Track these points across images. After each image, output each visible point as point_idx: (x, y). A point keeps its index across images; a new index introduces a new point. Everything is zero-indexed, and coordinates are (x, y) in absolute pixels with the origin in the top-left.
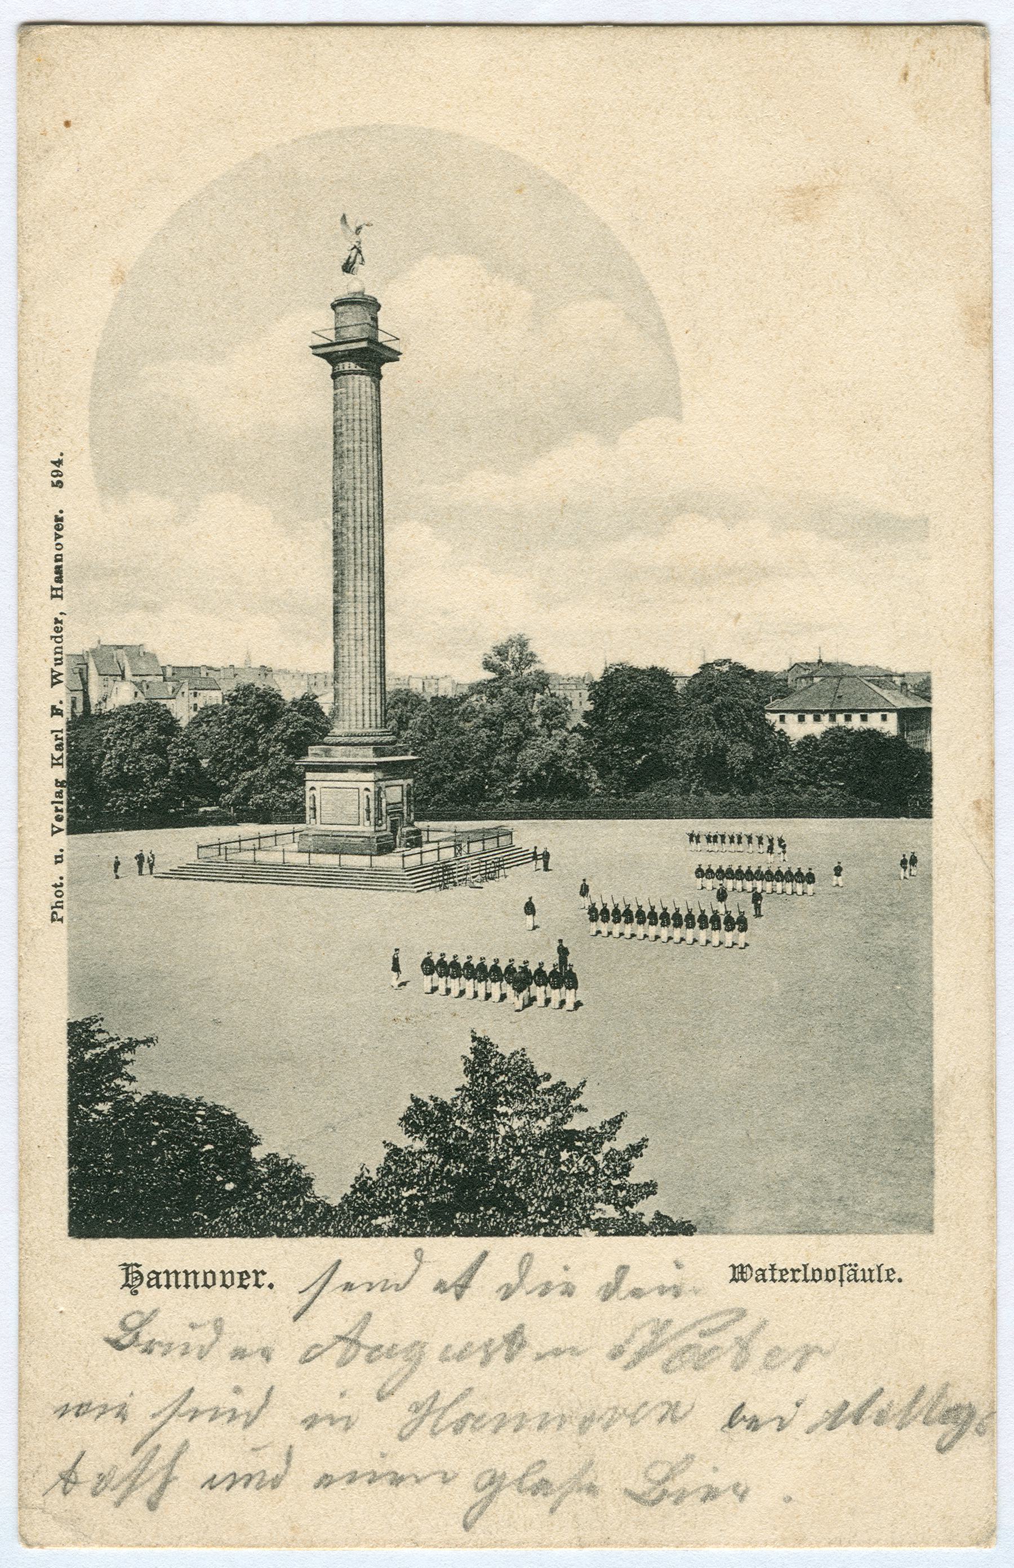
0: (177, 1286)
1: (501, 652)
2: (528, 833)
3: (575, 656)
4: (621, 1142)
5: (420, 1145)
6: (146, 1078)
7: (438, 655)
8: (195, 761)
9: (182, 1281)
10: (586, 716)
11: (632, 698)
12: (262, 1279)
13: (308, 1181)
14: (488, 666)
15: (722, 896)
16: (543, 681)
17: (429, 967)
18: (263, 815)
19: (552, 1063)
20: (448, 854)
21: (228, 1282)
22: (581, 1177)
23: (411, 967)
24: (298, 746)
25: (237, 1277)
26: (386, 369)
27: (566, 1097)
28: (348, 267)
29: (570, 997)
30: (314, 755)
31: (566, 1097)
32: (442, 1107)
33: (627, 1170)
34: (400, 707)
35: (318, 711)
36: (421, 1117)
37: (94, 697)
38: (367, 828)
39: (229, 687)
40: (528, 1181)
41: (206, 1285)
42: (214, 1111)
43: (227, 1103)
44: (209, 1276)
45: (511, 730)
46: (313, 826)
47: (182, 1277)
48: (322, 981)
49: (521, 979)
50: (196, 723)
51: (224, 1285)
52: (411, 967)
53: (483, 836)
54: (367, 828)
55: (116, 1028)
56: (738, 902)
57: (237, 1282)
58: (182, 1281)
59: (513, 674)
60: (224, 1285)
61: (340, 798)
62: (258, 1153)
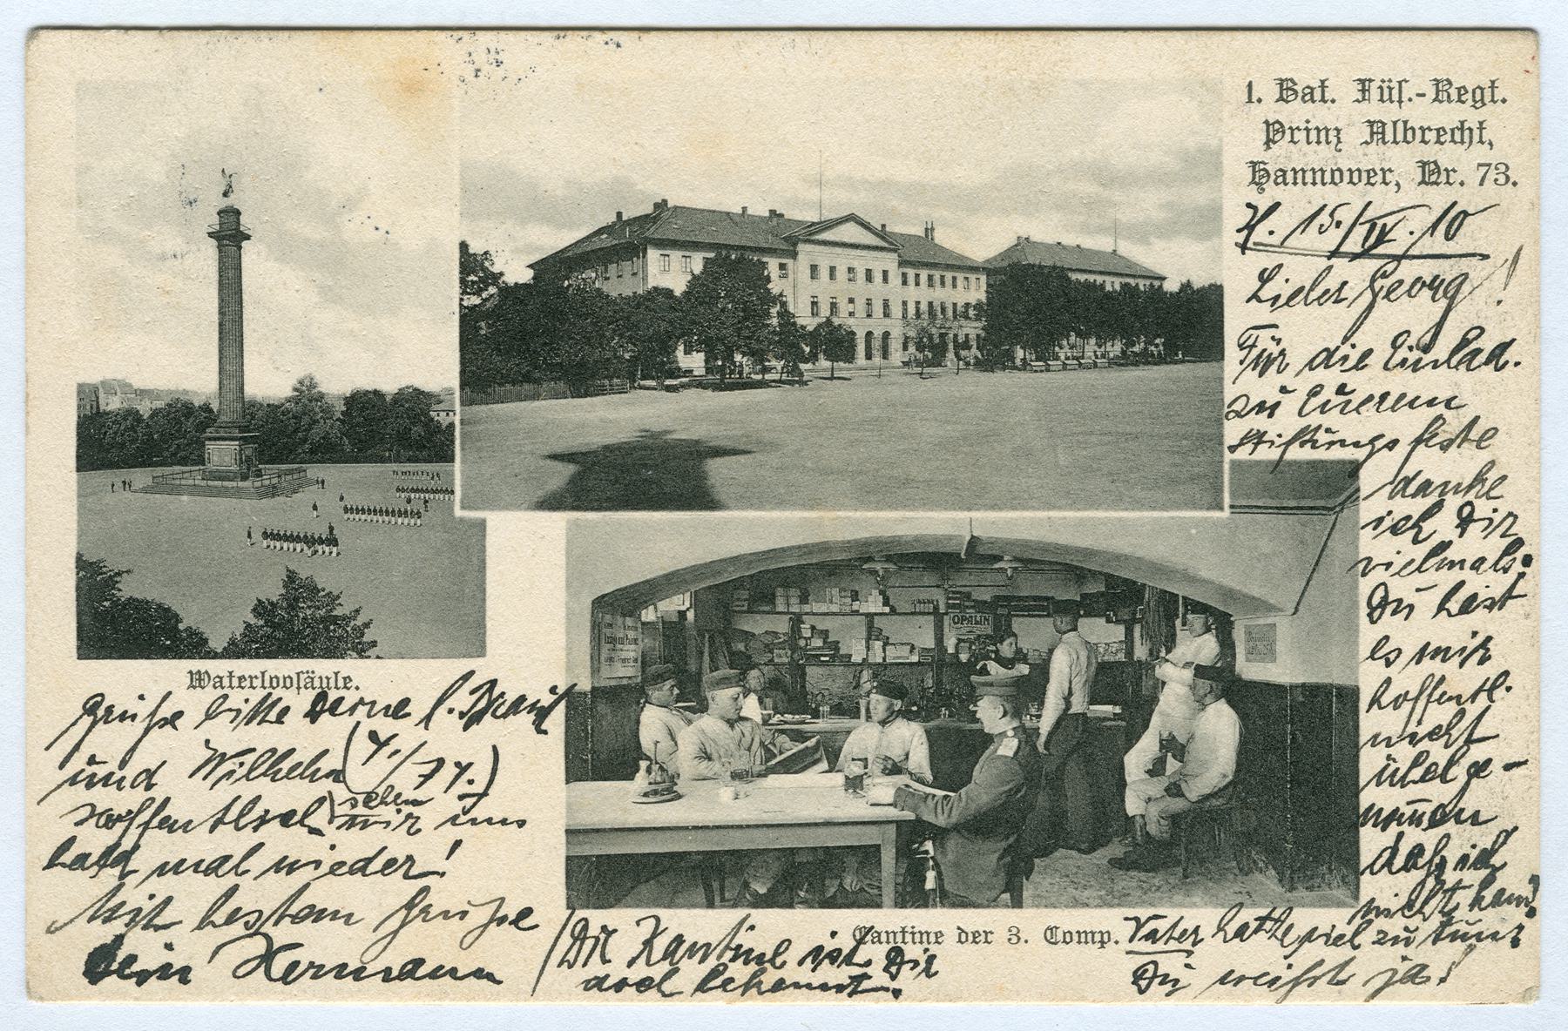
0: (1305, 184)
1: (301, 383)
2: (314, 471)
3: (338, 383)
4: (359, 622)
5: (261, 622)
6: (128, 589)
7: (268, 381)
8: (151, 434)
9: (1309, 178)
10: (343, 413)
11: (364, 404)
12: (1389, 176)
13: (206, 641)
14: (296, 390)
15: (409, 501)
16: (321, 396)
17: (266, 535)
18: (183, 462)
19: (326, 582)
20: (275, 481)
21: (1355, 180)
22: (340, 638)
23: (257, 536)
24: (202, 427)
25: (1364, 175)
26: (244, 244)
27: (333, 599)
28: (225, 194)
29: (335, 550)
30: (210, 432)
31: (333, 599)
32: (272, 604)
33: (363, 635)
34: (250, 409)
35: (211, 411)
36: (261, 609)
37: (102, 402)
38: (235, 468)
39: (168, 400)
40: (314, 641)
41: (1332, 182)
42: (160, 606)
43: (167, 603)
44: (1337, 174)
45: (305, 420)
46: (210, 467)
47: (1309, 175)
48: (216, 538)
49: (310, 541)
50: (152, 417)
51: (1351, 182)
52: (257, 536)
53: (291, 472)
54: (235, 468)
55: (113, 564)
56: (417, 505)
57: (1364, 180)
58: (1309, 178)
59: (307, 394)
60: (1351, 182)
61: (222, 453)
62: (181, 626)
